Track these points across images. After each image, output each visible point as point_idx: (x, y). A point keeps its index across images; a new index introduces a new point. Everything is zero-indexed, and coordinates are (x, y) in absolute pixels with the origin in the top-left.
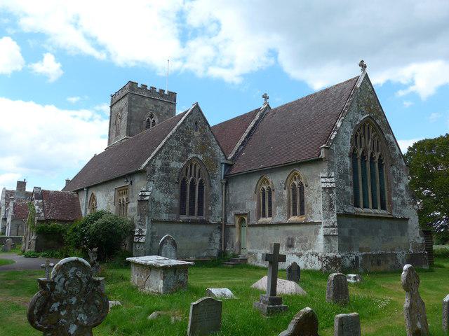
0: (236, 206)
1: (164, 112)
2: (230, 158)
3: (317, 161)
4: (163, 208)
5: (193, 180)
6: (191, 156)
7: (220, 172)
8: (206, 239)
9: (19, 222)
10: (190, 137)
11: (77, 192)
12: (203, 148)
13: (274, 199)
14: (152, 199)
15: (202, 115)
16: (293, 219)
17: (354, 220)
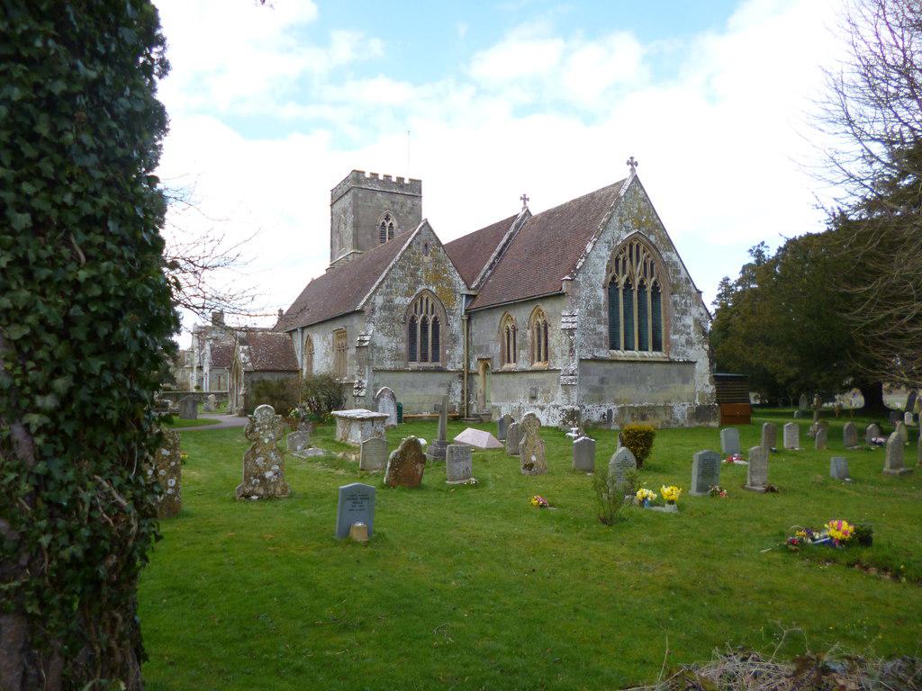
0: (480, 349)
1: (405, 210)
2: (473, 286)
3: (559, 295)
4: (387, 353)
5: (424, 318)
6: (421, 288)
7: (460, 306)
8: (443, 392)
9: (219, 371)
10: (418, 264)
11: (290, 332)
12: (437, 277)
13: (518, 342)
14: (373, 345)
15: (434, 234)
16: (537, 365)
17: (607, 366)
